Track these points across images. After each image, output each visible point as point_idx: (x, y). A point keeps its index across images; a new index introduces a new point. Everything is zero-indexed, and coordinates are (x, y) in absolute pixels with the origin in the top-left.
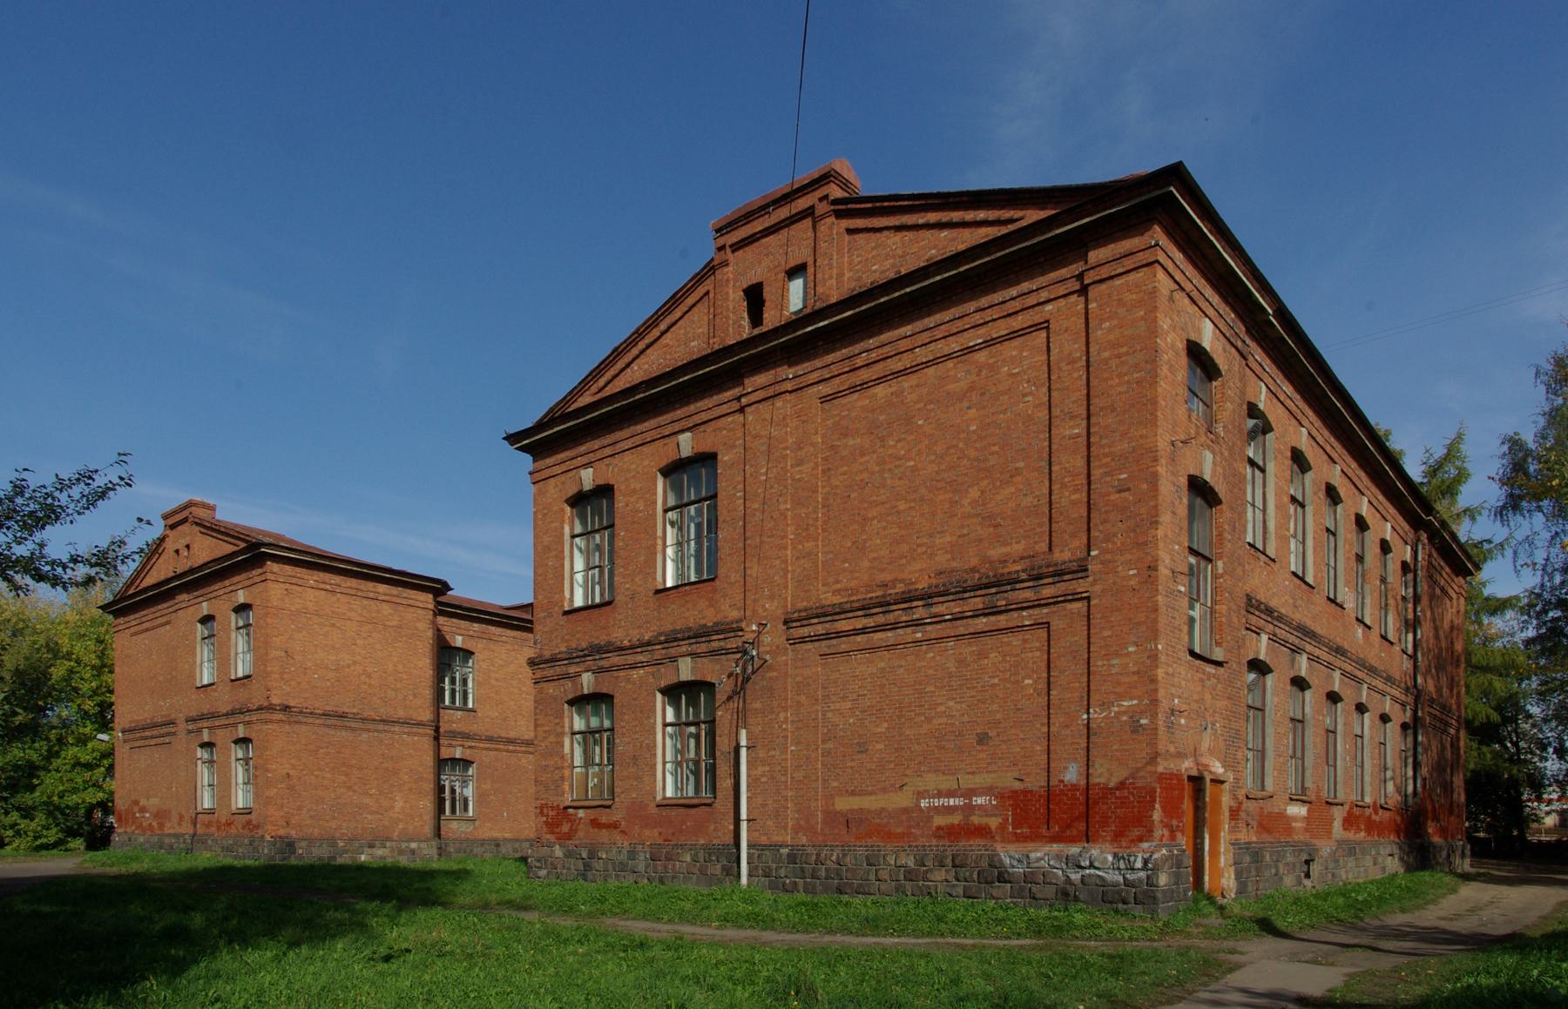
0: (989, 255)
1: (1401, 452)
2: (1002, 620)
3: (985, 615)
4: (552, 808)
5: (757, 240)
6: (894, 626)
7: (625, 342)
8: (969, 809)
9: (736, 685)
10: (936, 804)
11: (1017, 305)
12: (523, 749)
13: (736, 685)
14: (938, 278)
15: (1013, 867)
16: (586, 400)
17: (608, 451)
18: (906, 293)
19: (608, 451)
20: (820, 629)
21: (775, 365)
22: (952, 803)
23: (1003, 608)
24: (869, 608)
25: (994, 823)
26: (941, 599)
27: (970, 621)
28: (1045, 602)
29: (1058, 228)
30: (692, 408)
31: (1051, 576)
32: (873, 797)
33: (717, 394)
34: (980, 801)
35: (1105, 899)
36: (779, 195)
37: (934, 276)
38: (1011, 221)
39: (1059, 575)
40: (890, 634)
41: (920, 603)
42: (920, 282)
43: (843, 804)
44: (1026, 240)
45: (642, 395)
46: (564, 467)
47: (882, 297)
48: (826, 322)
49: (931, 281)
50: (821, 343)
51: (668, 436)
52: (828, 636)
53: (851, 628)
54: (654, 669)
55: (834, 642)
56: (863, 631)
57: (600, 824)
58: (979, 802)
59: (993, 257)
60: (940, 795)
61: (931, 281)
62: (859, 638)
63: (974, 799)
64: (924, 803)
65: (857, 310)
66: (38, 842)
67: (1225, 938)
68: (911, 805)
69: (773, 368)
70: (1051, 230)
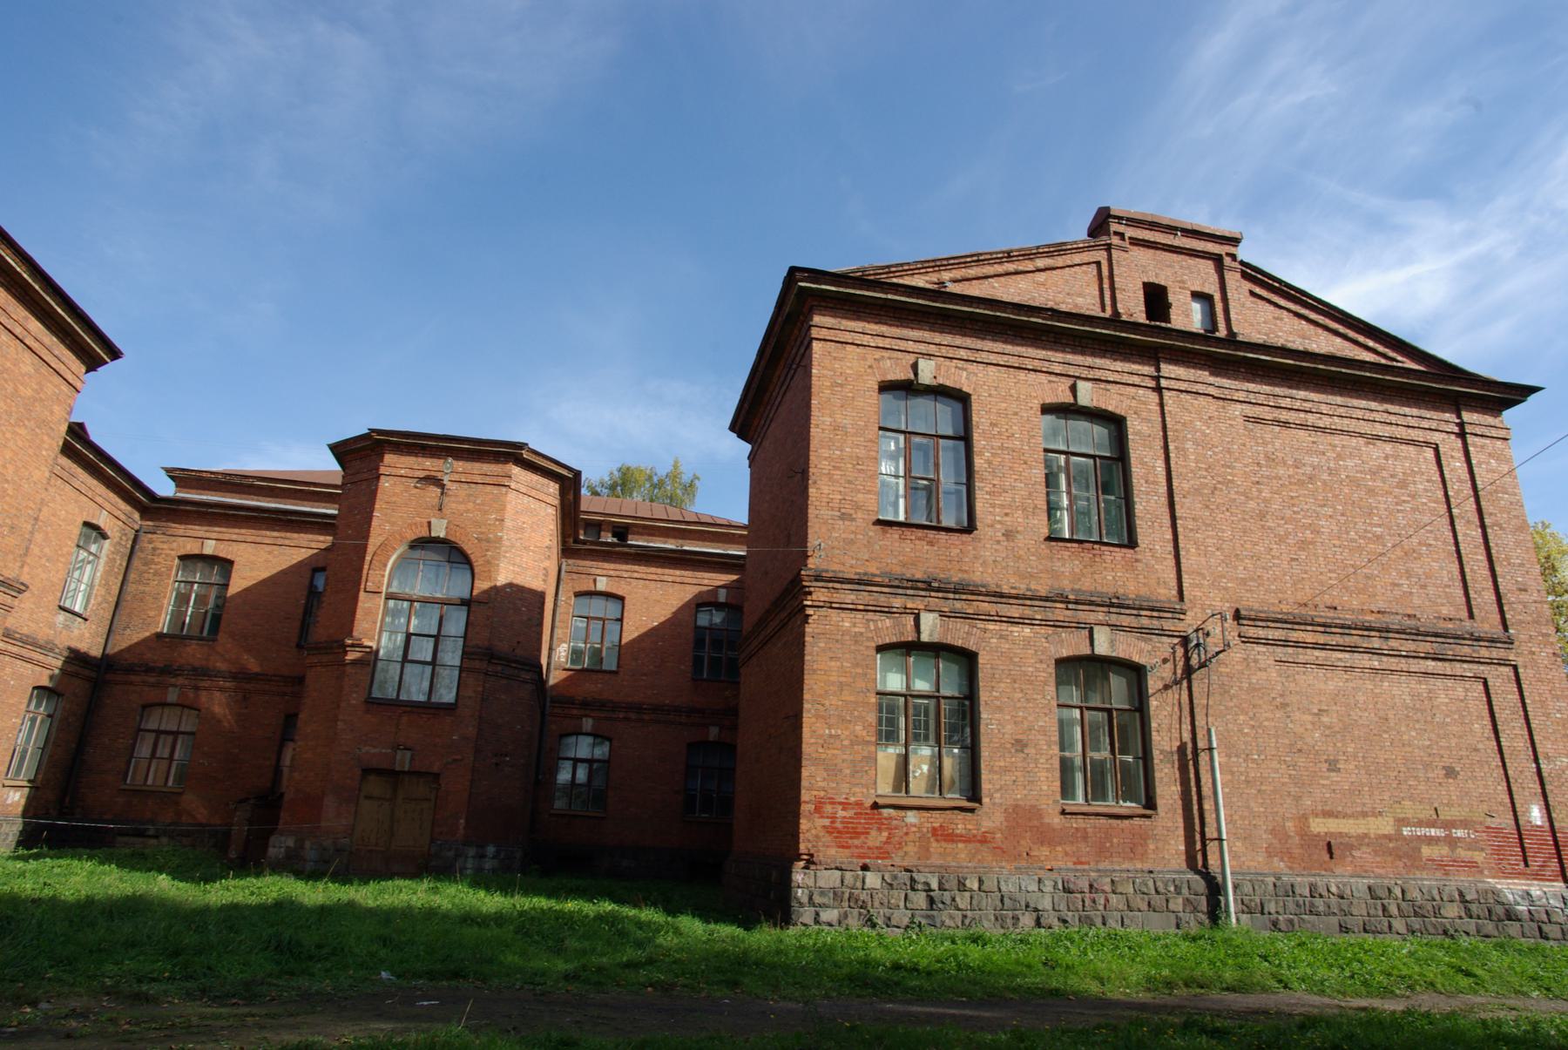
0: (1408, 378)
1: (885, 532)
2: (1446, 668)
3: (1434, 659)
4: (845, 805)
5: (1157, 249)
6: (1353, 649)
7: (991, 254)
8: (1452, 842)
9: (1175, 673)
10: (1419, 834)
11: (1359, 414)
12: (15, 649)
13: (1175, 673)
14: (1368, 374)
15: (1519, 904)
16: (919, 281)
17: (963, 353)
18: (1341, 372)
19: (963, 353)
20: (1278, 634)
21: (1196, 366)
22: (1433, 830)
23: (1450, 657)
24: (1330, 627)
25: (1479, 857)
26: (1397, 636)
27: (1422, 661)
28: (1171, 633)
29: (1457, 386)
30: (1098, 362)
31: (1488, 641)
32: (1351, 821)
33: (1121, 361)
34: (1460, 833)
35: (1368, 928)
36: (1190, 228)
37: (1365, 371)
38: (1397, 361)
39: (1493, 641)
40: (1347, 655)
41: (1377, 634)
42: (1354, 369)
43: (1319, 826)
44: (854, 288)
45: (1040, 321)
46: (880, 342)
47: (1321, 364)
48: (833, 288)
49: (1363, 373)
50: (1243, 370)
51: (1057, 374)
52: (1285, 643)
53: (1314, 641)
54: (1050, 630)
55: (1290, 650)
56: (1323, 647)
57: (952, 835)
58: (1459, 835)
59: (1410, 381)
60: (1420, 824)
61: (1363, 373)
62: (1317, 653)
63: (1454, 831)
64: (1406, 831)
65: (1298, 363)
66: (1291, 894)
67: (32, 940)
68: (1393, 832)
69: (1193, 368)
70: (1451, 385)
